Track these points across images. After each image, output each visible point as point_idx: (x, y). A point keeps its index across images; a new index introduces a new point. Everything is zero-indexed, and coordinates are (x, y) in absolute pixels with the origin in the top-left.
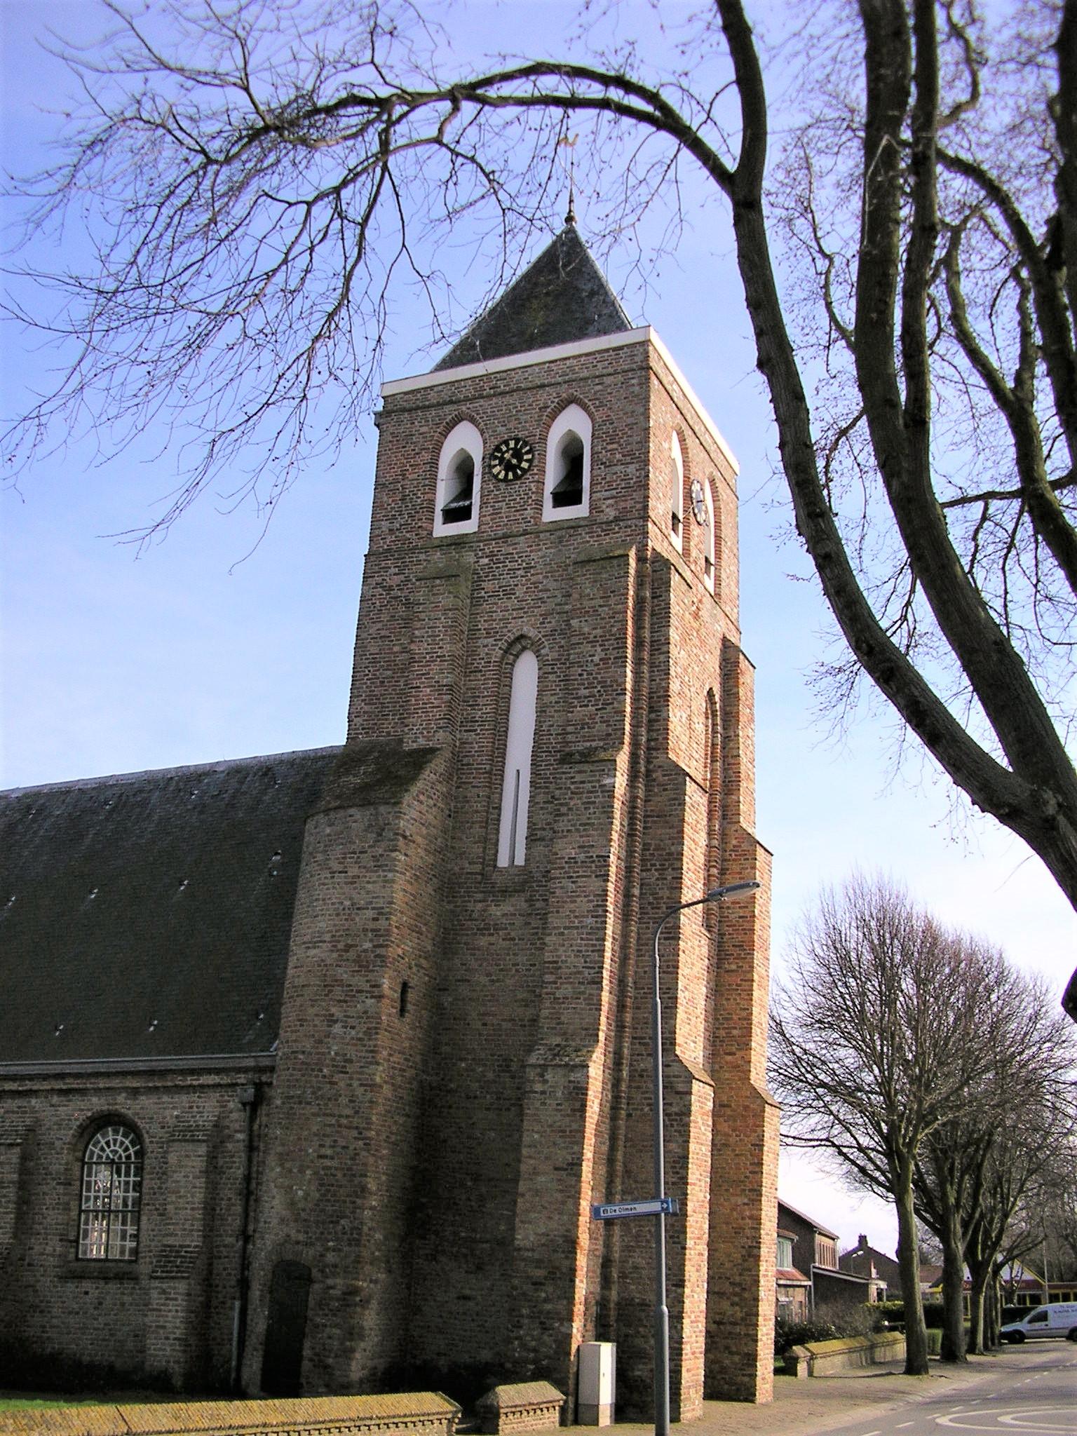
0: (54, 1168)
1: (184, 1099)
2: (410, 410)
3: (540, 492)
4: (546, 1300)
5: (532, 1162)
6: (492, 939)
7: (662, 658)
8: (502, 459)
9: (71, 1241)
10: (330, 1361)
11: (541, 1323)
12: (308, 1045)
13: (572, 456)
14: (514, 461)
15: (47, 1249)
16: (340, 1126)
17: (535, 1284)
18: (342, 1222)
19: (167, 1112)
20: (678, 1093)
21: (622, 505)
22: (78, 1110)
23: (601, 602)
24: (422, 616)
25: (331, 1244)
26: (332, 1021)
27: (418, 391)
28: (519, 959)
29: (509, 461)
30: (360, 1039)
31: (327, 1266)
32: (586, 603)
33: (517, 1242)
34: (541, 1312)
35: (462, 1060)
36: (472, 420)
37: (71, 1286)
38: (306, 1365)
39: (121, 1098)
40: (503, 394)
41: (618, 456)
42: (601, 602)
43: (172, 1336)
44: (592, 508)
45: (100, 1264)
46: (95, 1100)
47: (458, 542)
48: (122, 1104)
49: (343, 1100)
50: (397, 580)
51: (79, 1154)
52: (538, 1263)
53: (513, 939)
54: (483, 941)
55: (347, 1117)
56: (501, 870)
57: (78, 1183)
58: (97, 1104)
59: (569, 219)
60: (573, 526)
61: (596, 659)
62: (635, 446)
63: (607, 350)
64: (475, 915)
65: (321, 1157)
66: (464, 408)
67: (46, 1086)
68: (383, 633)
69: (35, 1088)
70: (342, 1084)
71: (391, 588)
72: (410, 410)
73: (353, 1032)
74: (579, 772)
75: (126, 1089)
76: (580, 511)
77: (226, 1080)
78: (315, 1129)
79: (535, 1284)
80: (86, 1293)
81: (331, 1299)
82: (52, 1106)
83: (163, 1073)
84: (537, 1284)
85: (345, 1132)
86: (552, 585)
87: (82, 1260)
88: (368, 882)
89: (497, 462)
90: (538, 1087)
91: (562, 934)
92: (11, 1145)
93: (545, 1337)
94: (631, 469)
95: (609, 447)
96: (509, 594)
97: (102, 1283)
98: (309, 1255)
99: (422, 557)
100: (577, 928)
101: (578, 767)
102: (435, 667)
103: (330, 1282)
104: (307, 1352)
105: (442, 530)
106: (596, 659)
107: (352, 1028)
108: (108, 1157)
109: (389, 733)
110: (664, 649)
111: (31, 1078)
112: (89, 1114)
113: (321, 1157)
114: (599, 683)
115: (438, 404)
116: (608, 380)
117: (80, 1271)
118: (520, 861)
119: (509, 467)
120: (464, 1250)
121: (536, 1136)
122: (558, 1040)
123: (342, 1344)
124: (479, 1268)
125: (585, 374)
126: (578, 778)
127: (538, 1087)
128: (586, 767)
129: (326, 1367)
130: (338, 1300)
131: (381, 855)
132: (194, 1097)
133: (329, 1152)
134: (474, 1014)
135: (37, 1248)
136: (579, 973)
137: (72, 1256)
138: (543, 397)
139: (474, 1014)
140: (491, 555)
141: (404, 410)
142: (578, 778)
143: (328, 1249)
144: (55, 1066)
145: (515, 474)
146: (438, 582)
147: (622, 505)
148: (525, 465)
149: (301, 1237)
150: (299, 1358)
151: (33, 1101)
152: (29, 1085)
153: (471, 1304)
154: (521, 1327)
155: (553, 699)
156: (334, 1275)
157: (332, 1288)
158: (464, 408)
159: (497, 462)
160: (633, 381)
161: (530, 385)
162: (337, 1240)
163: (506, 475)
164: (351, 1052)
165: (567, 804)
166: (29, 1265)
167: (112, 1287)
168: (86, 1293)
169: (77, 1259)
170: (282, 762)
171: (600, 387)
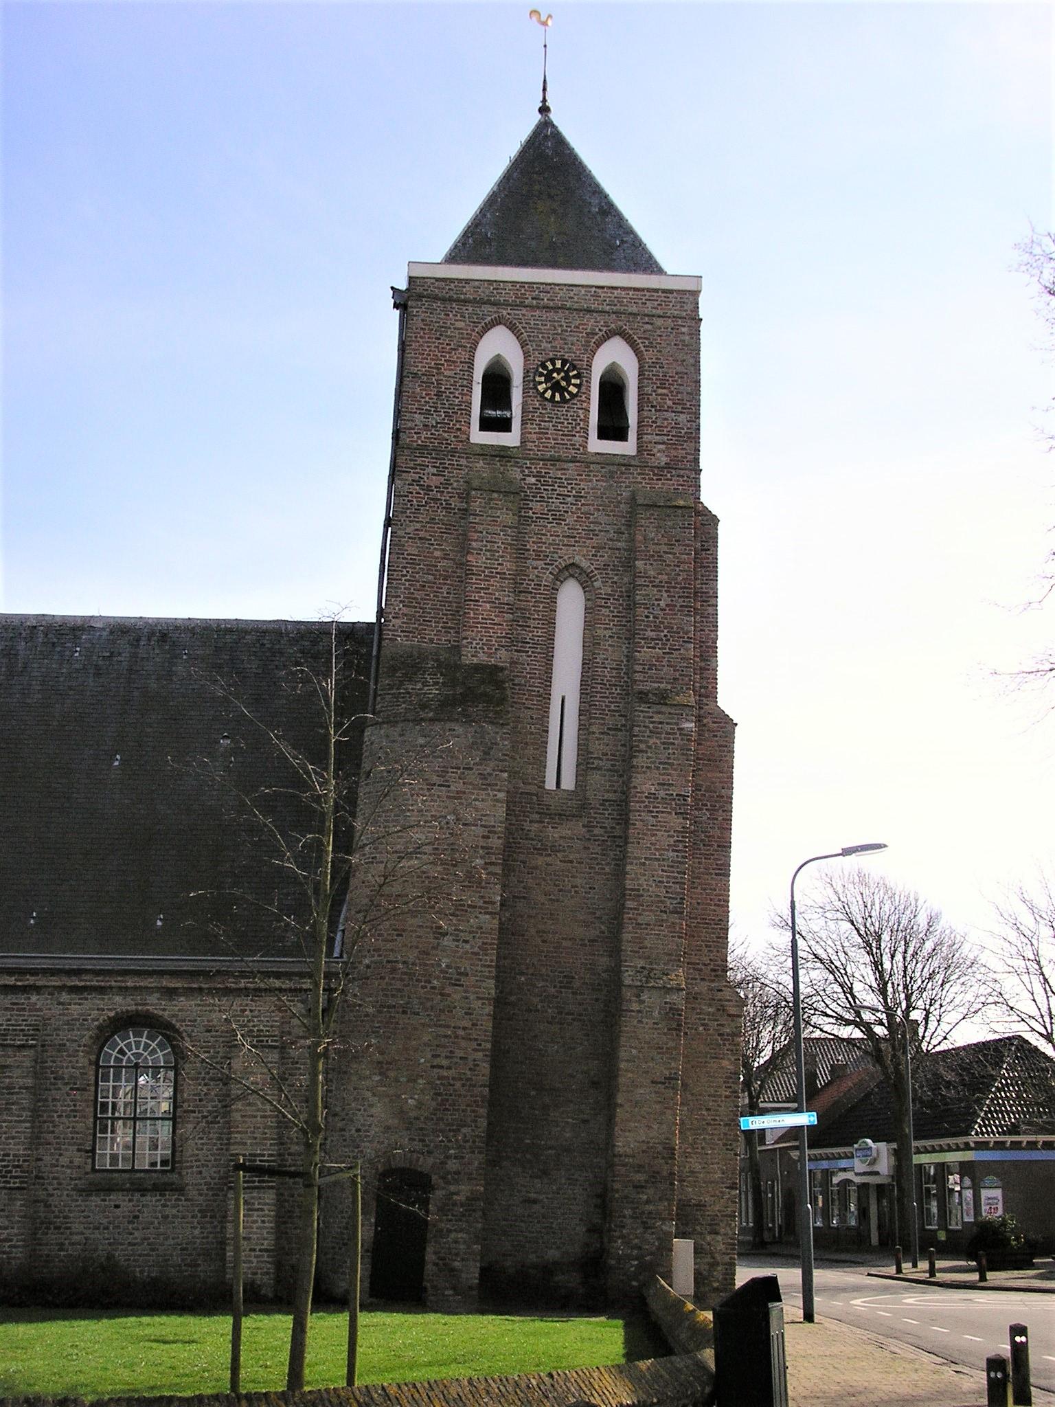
0: (67, 1072)
1: (238, 1003)
2: (444, 300)
3: (586, 420)
4: (648, 1202)
5: (630, 1075)
6: (548, 859)
7: (710, 610)
8: (548, 378)
9: (87, 1152)
10: (457, 1264)
11: (643, 1222)
12: (412, 956)
13: (612, 389)
14: (563, 384)
15: (65, 1161)
16: (457, 1037)
17: (635, 1187)
18: (464, 1130)
19: (213, 1016)
20: (729, 1015)
21: (674, 453)
22: (99, 1008)
23: (665, 548)
24: (480, 528)
25: (452, 1151)
26: (440, 933)
27: (452, 280)
28: (579, 881)
29: (558, 382)
30: (477, 954)
31: (449, 1173)
32: (652, 547)
33: (617, 1149)
34: (643, 1213)
35: (522, 974)
36: (512, 328)
37: (95, 1200)
38: (429, 1268)
39: (153, 999)
40: (547, 308)
41: (669, 403)
42: (665, 548)
43: (258, 1248)
44: (640, 448)
45: (127, 1176)
46: (118, 999)
47: (502, 454)
48: (155, 1004)
49: (459, 1013)
50: (436, 481)
51: (93, 1057)
52: (640, 1168)
53: (571, 862)
54: (540, 861)
55: (464, 1029)
56: (549, 792)
57: (93, 1088)
58: (121, 1004)
59: (544, 110)
60: (623, 463)
61: (662, 603)
62: (686, 397)
63: (656, 290)
64: (532, 835)
65: (433, 1067)
66: (505, 313)
67: (55, 982)
68: (422, 534)
69: (38, 983)
70: (456, 997)
71: (429, 489)
72: (444, 300)
73: (468, 946)
74: (659, 713)
75: (158, 989)
76: (627, 448)
77: (288, 984)
78: (426, 1039)
79: (635, 1187)
80: (117, 1206)
81: (454, 1204)
82: (60, 1003)
83: (205, 974)
84: (639, 1187)
85: (463, 1044)
86: (603, 519)
87: (99, 1171)
88: (476, 800)
89: (543, 379)
90: (635, 1007)
91: (644, 864)
92: (23, 1046)
93: (647, 1236)
94: (683, 418)
95: (660, 391)
96: (559, 519)
97: (137, 1196)
98: (425, 1163)
99: (463, 462)
100: (658, 860)
101: (656, 708)
102: (495, 583)
103: (452, 1188)
104: (430, 1256)
105: (479, 437)
106: (662, 603)
107: (466, 942)
108: (129, 1060)
109: (431, 641)
110: (712, 602)
111: (34, 972)
112: (112, 1014)
113: (433, 1067)
114: (665, 628)
115: (474, 301)
116: (659, 322)
117: (103, 1184)
118: (568, 783)
119: (556, 387)
120: (528, 1156)
121: (634, 1051)
122: (641, 963)
123: (469, 1247)
124: (545, 1173)
125: (634, 309)
126: (657, 718)
127: (635, 1006)
128: (664, 709)
129: (453, 1270)
130: (462, 1206)
131: (490, 775)
132: (247, 1000)
133: (445, 1062)
134: (533, 931)
135: (47, 1158)
136: (662, 902)
137: (89, 1168)
138: (591, 322)
139: (533, 931)
140: (538, 476)
141: (436, 298)
142: (657, 718)
143: (448, 1157)
144: (71, 960)
145: (562, 396)
146: (495, 495)
147: (674, 453)
148: (574, 390)
149: (418, 1145)
150: (422, 1263)
151: (34, 998)
152: (31, 980)
153: (536, 1207)
154: (623, 1227)
155: (608, 633)
156: (457, 1182)
157: (457, 1194)
158: (505, 313)
159: (543, 379)
160: (684, 330)
161: (576, 306)
162: (459, 1147)
163: (553, 396)
164: (465, 965)
165: (646, 742)
166: (37, 1177)
167: (150, 1199)
168: (117, 1206)
169: (94, 1170)
170: (177, 628)
171: (649, 327)
